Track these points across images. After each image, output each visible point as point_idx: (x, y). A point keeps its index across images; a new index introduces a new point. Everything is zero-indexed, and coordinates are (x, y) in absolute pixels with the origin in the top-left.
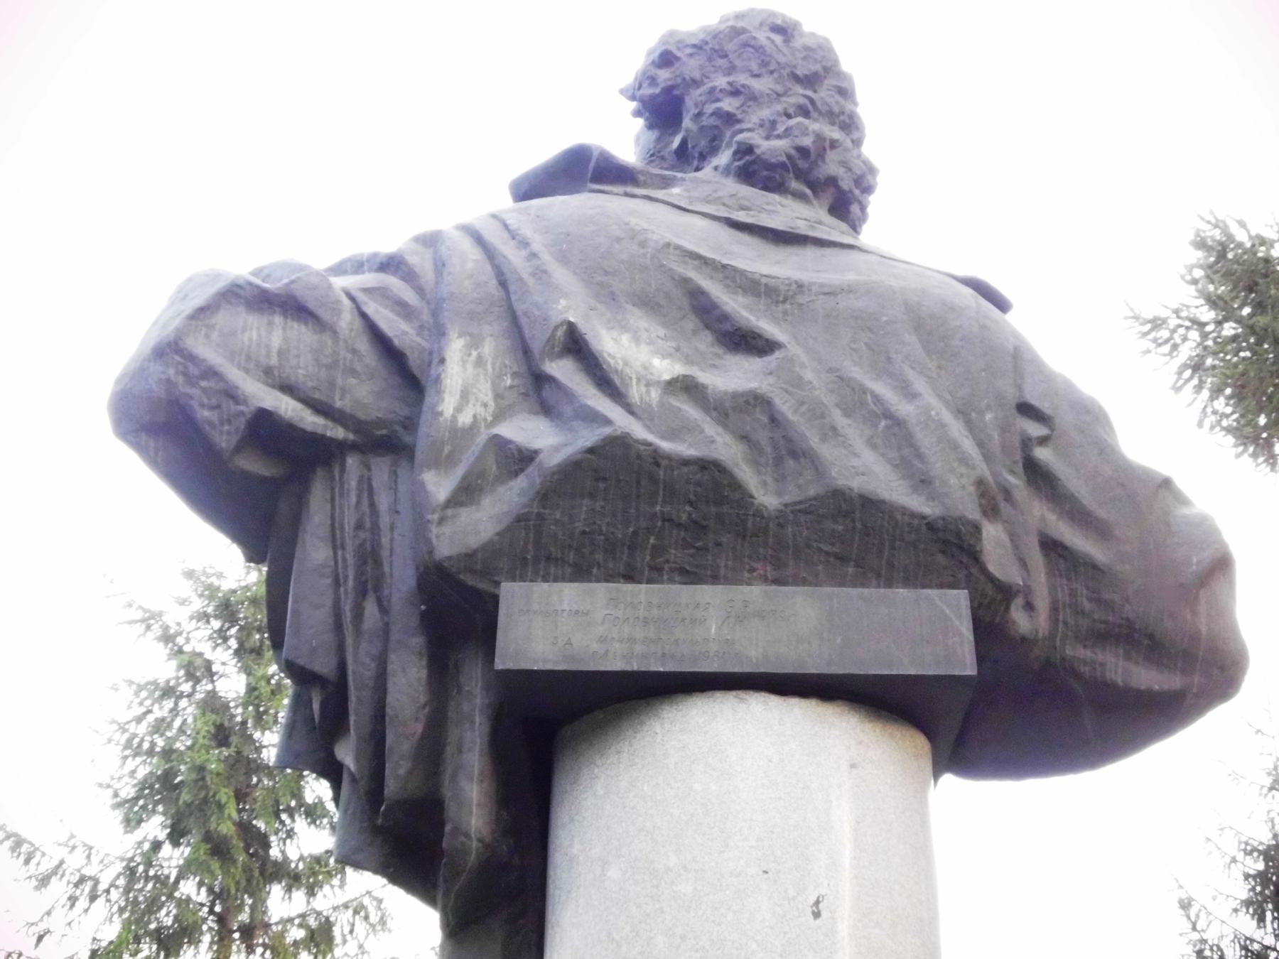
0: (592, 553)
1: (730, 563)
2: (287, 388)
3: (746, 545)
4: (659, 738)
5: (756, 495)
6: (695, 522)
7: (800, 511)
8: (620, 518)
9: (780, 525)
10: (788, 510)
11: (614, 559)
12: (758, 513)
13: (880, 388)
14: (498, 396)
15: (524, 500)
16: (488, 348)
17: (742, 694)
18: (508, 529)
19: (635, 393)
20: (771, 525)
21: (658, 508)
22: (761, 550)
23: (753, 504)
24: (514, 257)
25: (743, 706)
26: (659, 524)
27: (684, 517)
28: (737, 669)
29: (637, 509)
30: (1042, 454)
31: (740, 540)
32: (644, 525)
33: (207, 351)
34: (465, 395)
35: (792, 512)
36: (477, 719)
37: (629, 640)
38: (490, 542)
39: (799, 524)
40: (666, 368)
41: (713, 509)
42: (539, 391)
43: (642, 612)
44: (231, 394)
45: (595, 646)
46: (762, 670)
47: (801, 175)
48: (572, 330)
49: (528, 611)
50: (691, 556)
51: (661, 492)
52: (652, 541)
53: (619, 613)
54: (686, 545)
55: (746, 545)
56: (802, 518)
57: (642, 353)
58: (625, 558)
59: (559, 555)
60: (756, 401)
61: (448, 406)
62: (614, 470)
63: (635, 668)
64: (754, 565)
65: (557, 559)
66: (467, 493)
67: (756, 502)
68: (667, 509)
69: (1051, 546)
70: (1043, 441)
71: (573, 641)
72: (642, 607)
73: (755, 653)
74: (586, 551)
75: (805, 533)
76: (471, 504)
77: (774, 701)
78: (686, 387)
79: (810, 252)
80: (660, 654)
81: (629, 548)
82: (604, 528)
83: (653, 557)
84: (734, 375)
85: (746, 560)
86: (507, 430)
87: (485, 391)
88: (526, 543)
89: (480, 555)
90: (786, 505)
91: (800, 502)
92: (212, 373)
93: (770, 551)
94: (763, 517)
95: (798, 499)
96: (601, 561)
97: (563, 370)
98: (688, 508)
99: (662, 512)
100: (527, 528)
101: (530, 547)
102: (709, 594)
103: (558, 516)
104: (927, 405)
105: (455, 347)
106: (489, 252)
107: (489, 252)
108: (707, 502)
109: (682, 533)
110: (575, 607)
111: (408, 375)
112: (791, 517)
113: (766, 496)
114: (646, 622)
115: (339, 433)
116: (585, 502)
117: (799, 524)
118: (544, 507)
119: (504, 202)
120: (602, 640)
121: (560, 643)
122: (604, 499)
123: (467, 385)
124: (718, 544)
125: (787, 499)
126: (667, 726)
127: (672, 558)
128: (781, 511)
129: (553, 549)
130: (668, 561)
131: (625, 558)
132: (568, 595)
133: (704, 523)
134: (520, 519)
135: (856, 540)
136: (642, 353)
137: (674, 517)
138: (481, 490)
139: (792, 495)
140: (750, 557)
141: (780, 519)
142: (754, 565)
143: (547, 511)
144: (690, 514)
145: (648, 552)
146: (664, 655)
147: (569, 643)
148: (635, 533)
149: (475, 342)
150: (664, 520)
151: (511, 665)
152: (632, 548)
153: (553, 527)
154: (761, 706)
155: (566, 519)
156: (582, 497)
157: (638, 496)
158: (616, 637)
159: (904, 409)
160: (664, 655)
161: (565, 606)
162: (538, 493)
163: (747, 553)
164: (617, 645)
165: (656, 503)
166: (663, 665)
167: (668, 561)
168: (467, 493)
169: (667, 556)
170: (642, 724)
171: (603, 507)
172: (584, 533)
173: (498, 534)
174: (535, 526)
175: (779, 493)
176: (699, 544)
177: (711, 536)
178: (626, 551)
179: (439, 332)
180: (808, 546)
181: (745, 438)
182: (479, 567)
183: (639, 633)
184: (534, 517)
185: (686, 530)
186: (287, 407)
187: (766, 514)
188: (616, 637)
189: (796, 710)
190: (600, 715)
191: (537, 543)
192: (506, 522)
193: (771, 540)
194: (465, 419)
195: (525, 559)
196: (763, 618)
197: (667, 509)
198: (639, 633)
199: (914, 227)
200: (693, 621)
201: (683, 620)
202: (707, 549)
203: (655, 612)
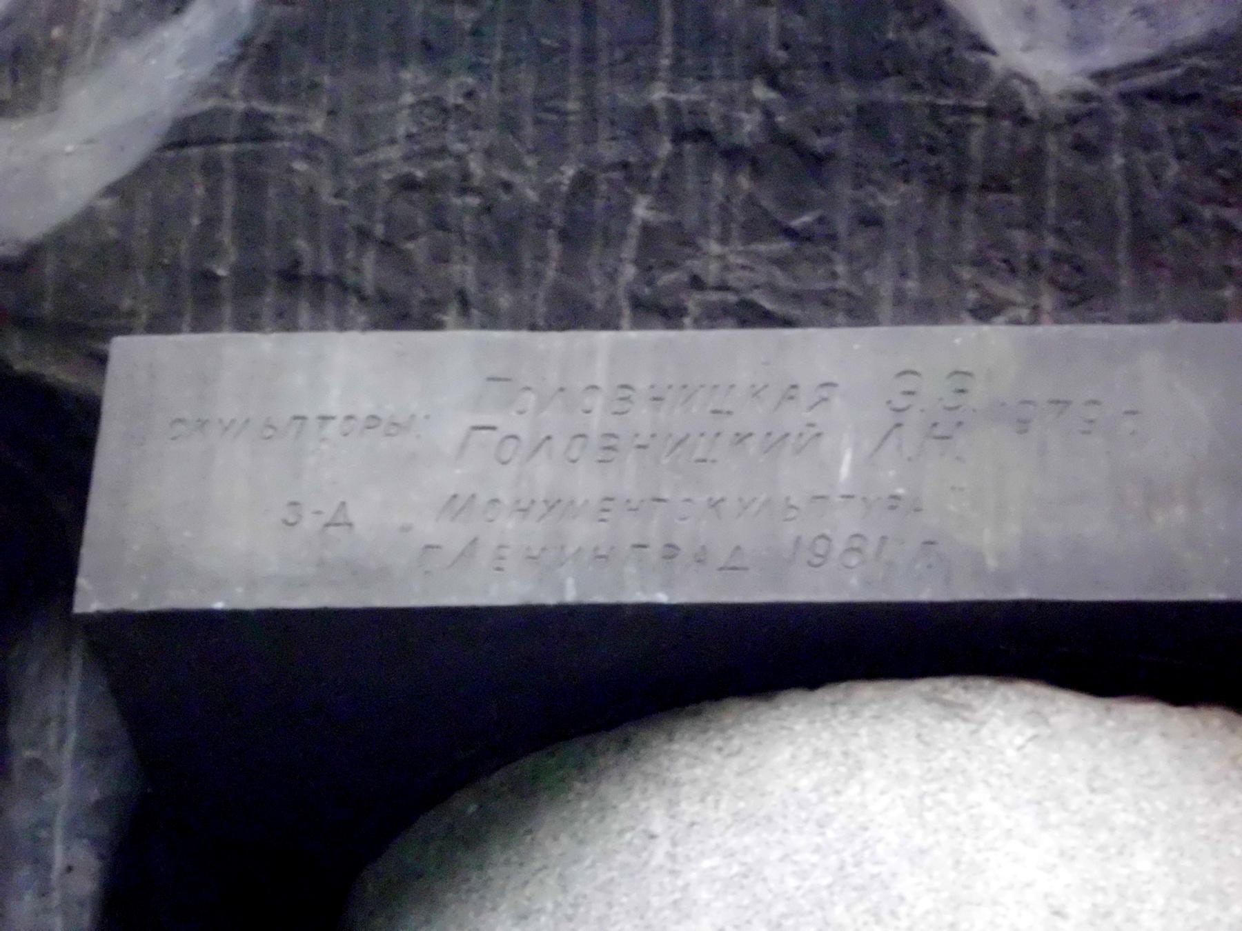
0: (441, 257)
1: (911, 285)
3: (969, 217)
4: (660, 851)
5: (994, 38)
6: (791, 142)
7: (1152, 94)
8: (529, 130)
9: (1086, 149)
10: (1111, 91)
11: (514, 272)
12: (1008, 107)
15: (202, 71)
17: (950, 688)
18: (145, 171)
20: (1052, 144)
21: (658, 94)
22: (1019, 237)
23: (983, 72)
25: (953, 731)
26: (665, 148)
27: (749, 125)
28: (927, 593)
29: (589, 100)
31: (943, 203)
32: (608, 151)
35: (1127, 98)
36: (59, 856)
37: (551, 505)
38: (88, 217)
39: (1148, 142)
41: (849, 94)
43: (596, 423)
45: (429, 529)
46: (1022, 593)
49: (202, 424)
50: (781, 262)
51: (667, 39)
52: (642, 210)
53: (508, 422)
54: (758, 226)
55: (969, 217)
56: (1158, 118)
58: (551, 273)
59: (328, 267)
63: (571, 596)
64: (999, 290)
65: (318, 280)
67: (997, 65)
68: (691, 94)
71: (355, 514)
72: (597, 403)
74: (418, 249)
75: (1173, 170)
76: (30, 108)
77: (1069, 711)
80: (656, 546)
81: (564, 236)
82: (476, 166)
83: (646, 270)
85: (966, 274)
88: (210, 223)
89: (50, 267)
90: (1102, 76)
91: (1153, 63)
93: (1051, 242)
94: (1022, 120)
95: (1142, 52)
96: (471, 287)
98: (761, 92)
99: (673, 107)
100: (211, 168)
101: (226, 236)
103: (318, 125)
108: (827, 66)
109: (744, 182)
110: (365, 408)
112: (1121, 116)
114: (610, 447)
116: (406, 75)
117: (1148, 142)
118: (272, 95)
120: (456, 506)
121: (310, 524)
122: (473, 68)
124: (869, 220)
125: (1108, 56)
126: (689, 809)
127: (711, 272)
128: (1085, 97)
129: (302, 244)
130: (696, 283)
131: (551, 273)
133: (819, 144)
134: (185, 136)
137: (714, 120)
138: (61, 63)
139: (1123, 43)
140: (979, 262)
141: (1084, 121)
142: (999, 290)
143: (281, 110)
144: (768, 114)
145: (629, 250)
146: (671, 551)
147: (340, 521)
148: (584, 182)
150: (680, 137)
151: (133, 597)
152: (574, 236)
153: (300, 166)
154: (1017, 736)
155: (345, 139)
156: (400, 60)
157: (589, 54)
158: (506, 498)
160: (671, 551)
161: (333, 405)
162: (245, 43)
163: (969, 246)
164: (509, 524)
165: (652, 74)
166: (666, 586)
167: (696, 283)
169: (696, 265)
170: (604, 810)
171: (469, 95)
172: (408, 185)
173: (112, 190)
174: (237, 159)
175: (1079, 42)
176: (801, 221)
177: (844, 189)
178: (554, 247)
180: (1185, 219)
182: (47, 307)
183: (587, 484)
184: (233, 129)
185: (758, 171)
187: (1031, 108)
188: (506, 498)
189: (1152, 743)
190: (467, 804)
191: (249, 225)
192: (139, 149)
193: (1052, 203)
195: (210, 278)
196: (1023, 425)
197: (691, 94)
198: (587, 484)
200: (775, 443)
201: (741, 438)
202: (832, 238)
203: (642, 417)
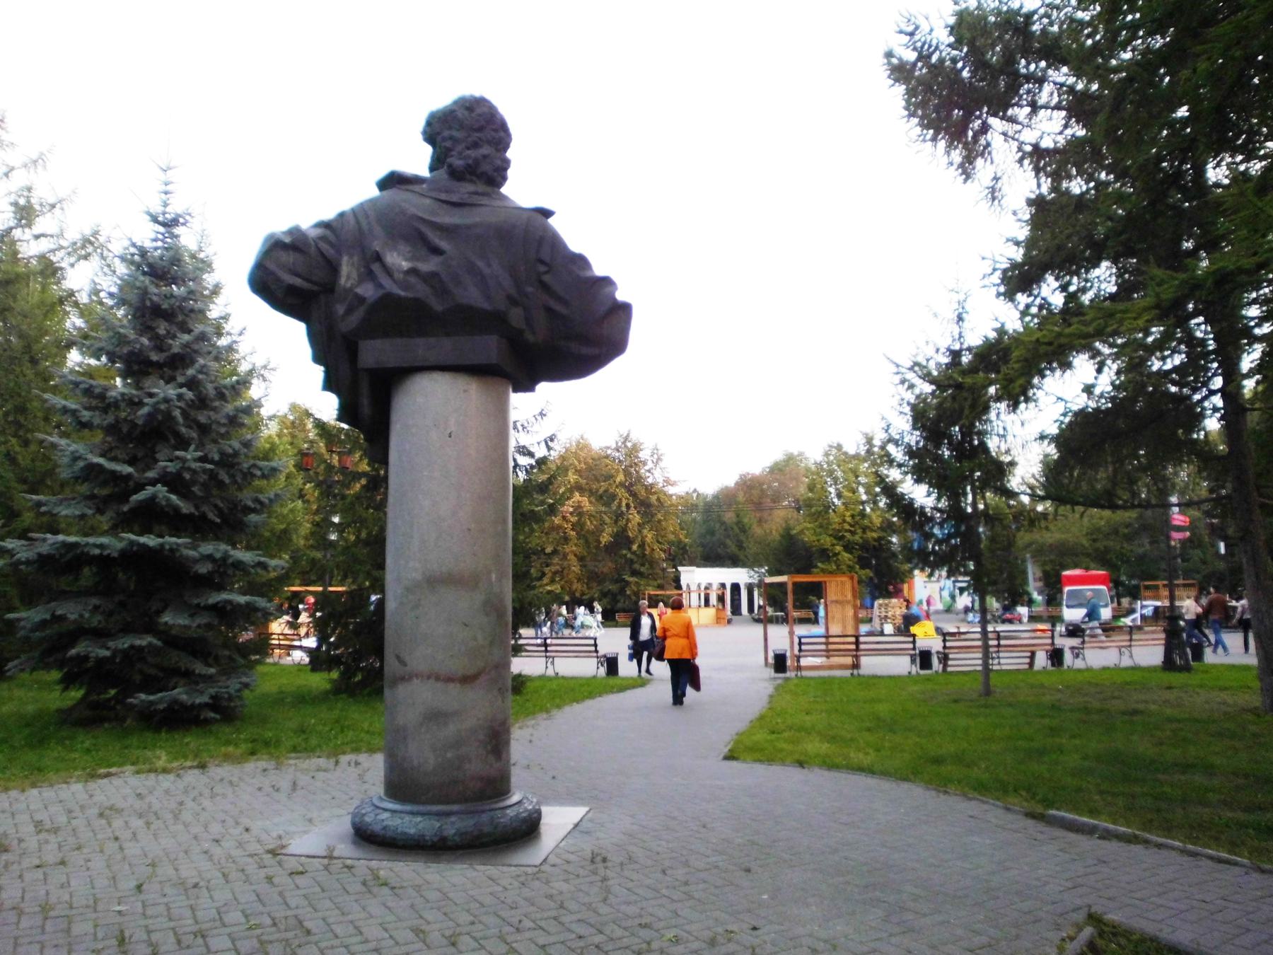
2: (298, 275)
13: (480, 264)
14: (359, 276)
16: (356, 258)
19: (396, 275)
24: (364, 224)
30: (547, 278)
33: (272, 266)
34: (348, 277)
40: (405, 265)
42: (369, 275)
44: (278, 280)
47: (471, 174)
48: (377, 253)
57: (398, 260)
60: (434, 275)
61: (343, 281)
62: (387, 301)
66: (349, 311)
69: (549, 310)
70: (546, 273)
73: (432, 359)
78: (413, 271)
79: (465, 210)
84: (427, 266)
86: (359, 291)
87: (355, 275)
92: (273, 273)
97: (376, 267)
102: (420, 341)
104: (494, 269)
105: (345, 259)
106: (358, 222)
107: (358, 222)
111: (334, 268)
113: (438, 306)
115: (315, 288)
119: (375, 192)
123: (348, 272)
132: (378, 343)
135: (467, 320)
136: (398, 260)
149: (351, 256)
159: (487, 271)
168: (349, 311)
179: (339, 253)
181: (432, 287)
186: (298, 282)
194: (349, 285)
199: (521, 188)
